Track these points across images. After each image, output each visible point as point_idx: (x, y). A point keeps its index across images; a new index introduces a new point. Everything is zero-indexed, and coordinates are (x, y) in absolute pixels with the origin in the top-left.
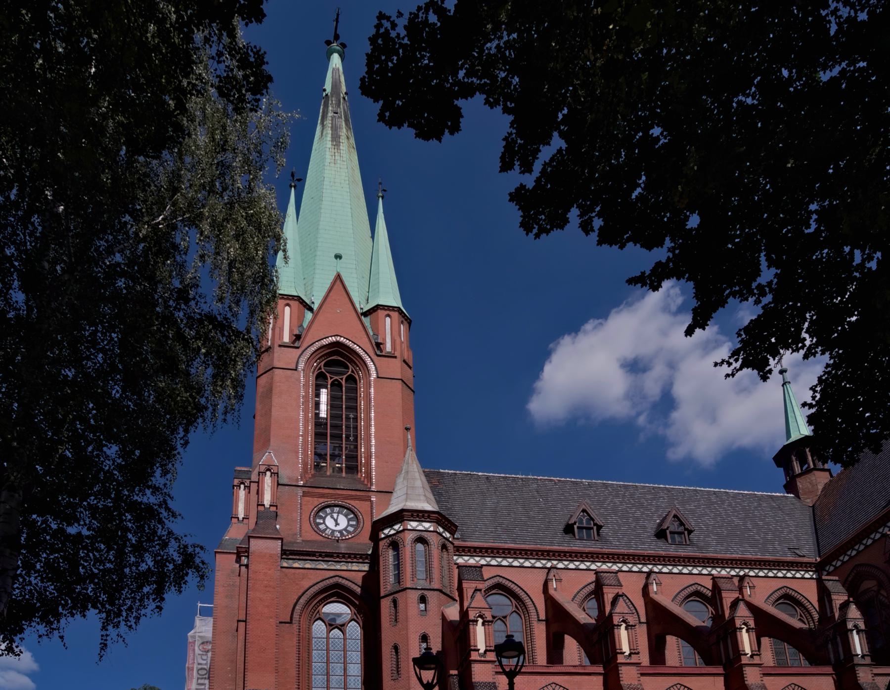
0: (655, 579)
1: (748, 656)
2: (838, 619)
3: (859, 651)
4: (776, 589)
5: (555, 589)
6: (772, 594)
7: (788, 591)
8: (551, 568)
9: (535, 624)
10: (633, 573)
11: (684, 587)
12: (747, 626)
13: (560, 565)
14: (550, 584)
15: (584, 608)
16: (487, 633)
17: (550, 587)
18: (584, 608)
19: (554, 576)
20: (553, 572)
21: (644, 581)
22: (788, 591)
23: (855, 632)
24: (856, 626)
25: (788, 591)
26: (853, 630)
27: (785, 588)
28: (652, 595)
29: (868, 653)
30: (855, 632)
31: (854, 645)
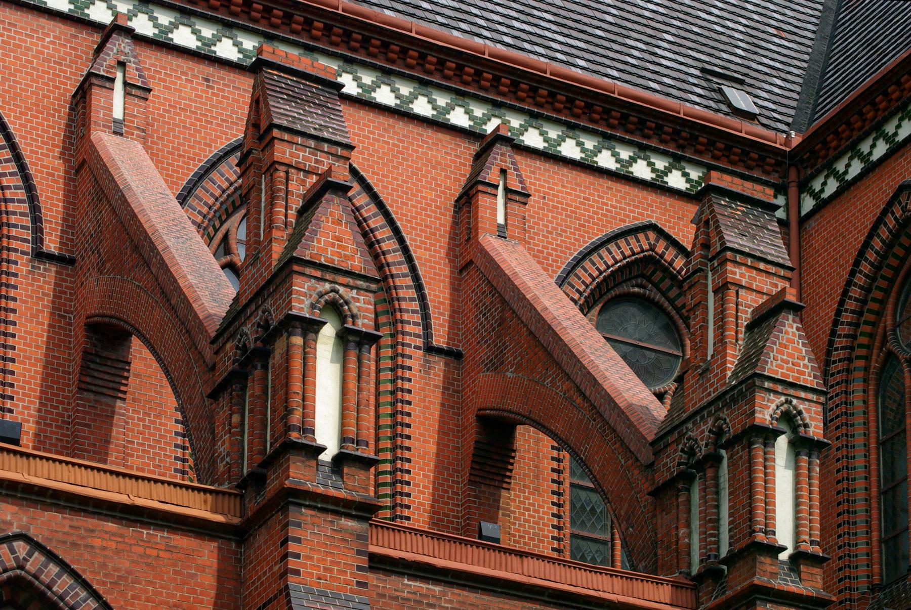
0: (122, 64)
1: (784, 556)
2: (735, 374)
3: (784, 535)
4: (617, 227)
5: (502, 232)
6: (595, 248)
7: (660, 247)
8: (498, 138)
9: (416, 359)
10: (43, 21)
11: (623, 226)
12: (794, 428)
13: (533, 139)
14: (97, 95)
15: (226, 237)
16: (352, 404)
17: (97, 115)
18: (226, 237)
19: (503, 172)
20: (500, 156)
21: (467, 170)
22: (660, 249)
23: (782, 442)
24: (789, 418)
25: (660, 249)
26: (777, 433)
27: (652, 235)
28: (490, 241)
29: (816, 550)
30: (782, 442)
31: (769, 501)
